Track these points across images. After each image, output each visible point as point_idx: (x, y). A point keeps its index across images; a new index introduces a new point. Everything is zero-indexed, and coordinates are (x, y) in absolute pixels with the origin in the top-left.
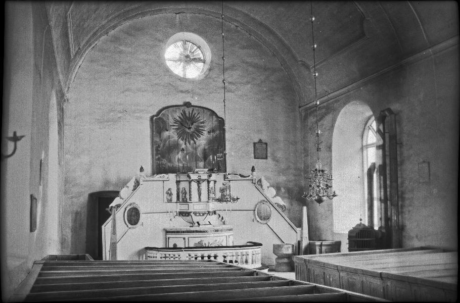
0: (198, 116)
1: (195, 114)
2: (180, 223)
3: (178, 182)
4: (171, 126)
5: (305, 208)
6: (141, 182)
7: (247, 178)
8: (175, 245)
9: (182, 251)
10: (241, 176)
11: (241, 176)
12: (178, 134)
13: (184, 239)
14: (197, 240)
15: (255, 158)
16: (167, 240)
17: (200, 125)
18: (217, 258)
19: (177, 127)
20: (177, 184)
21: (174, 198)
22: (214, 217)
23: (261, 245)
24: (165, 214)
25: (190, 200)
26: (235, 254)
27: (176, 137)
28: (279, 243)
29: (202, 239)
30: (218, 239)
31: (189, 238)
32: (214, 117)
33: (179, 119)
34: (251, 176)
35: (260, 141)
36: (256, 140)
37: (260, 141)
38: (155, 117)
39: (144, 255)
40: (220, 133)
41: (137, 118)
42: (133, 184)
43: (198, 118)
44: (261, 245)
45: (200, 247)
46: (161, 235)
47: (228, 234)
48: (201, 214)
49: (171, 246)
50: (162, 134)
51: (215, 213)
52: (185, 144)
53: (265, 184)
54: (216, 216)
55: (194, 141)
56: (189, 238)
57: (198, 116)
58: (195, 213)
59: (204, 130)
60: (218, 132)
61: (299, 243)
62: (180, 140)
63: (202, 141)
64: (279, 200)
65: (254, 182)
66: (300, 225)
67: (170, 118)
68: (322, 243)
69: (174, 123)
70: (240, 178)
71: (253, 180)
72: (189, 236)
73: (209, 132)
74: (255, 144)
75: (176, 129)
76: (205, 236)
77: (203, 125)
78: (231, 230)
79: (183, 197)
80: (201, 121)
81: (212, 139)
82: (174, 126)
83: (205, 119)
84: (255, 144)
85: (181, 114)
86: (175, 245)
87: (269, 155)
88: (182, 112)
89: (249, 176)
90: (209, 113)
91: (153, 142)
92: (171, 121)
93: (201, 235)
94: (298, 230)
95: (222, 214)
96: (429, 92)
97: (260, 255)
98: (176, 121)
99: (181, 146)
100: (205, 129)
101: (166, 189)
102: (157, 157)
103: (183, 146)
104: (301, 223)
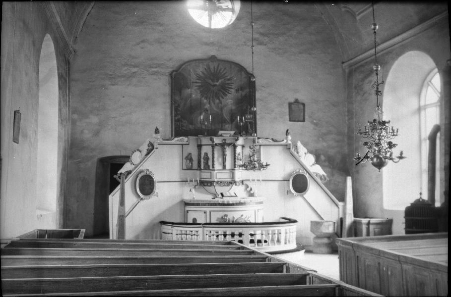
0: (225, 72)
5: (349, 180)
8: (195, 220)
13: (205, 212)
15: (290, 120)
17: (227, 82)
19: (200, 84)
27: (199, 96)
29: (226, 213)
32: (243, 73)
34: (285, 141)
35: (297, 101)
36: (292, 100)
38: (174, 73)
40: (250, 92)
42: (147, 147)
43: (225, 74)
44: (295, 221)
49: (190, 221)
52: (209, 103)
55: (220, 100)
59: (232, 88)
60: (247, 90)
62: (203, 98)
66: (342, 199)
69: (198, 79)
70: (273, 143)
73: (237, 91)
75: (198, 86)
77: (229, 82)
78: (261, 203)
80: (229, 77)
82: (196, 82)
83: (232, 76)
84: (290, 104)
86: (195, 220)
94: (341, 204)
95: (250, 185)
98: (199, 78)
100: (233, 87)
102: (176, 118)
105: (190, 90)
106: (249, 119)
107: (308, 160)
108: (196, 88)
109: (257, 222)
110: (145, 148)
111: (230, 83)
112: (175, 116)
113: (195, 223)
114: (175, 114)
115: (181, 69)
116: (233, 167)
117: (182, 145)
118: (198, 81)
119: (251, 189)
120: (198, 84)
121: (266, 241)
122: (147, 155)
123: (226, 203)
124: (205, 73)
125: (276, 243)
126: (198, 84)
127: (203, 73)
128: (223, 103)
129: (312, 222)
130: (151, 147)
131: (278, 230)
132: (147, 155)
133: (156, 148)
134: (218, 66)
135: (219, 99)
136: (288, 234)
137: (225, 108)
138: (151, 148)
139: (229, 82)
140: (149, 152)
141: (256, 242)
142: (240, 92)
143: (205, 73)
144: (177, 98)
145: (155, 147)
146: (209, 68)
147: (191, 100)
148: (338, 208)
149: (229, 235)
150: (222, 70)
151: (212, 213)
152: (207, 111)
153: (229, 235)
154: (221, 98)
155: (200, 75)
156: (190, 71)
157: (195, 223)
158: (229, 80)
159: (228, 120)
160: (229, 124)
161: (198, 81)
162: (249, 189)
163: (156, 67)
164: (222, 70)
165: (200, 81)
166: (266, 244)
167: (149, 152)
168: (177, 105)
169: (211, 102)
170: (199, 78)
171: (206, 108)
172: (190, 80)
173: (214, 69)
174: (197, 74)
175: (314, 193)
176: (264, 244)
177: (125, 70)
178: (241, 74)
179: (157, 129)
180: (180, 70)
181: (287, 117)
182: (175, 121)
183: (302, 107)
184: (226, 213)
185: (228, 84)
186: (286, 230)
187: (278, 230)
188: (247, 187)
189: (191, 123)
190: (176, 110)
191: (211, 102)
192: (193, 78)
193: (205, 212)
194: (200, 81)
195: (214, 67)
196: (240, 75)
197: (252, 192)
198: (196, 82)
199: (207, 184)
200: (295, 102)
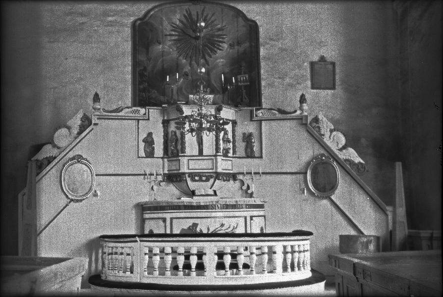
0: (213, 18)
1: (207, 16)
2: (169, 193)
3: (166, 123)
4: (166, 35)
5: (399, 166)
6: (94, 120)
7: (289, 116)
8: (151, 231)
9: (136, 241)
10: (281, 111)
11: (281, 111)
12: (178, 48)
13: (164, 220)
14: (186, 224)
15: (313, 88)
16: (142, 222)
17: (216, 33)
18: (204, 257)
19: (176, 37)
20: (164, 126)
21: (159, 150)
22: (233, 185)
23: (310, 234)
24: (142, 177)
25: (183, 153)
26: (266, 250)
27: (175, 55)
28: (353, 233)
29: (196, 221)
30: (226, 221)
31: (172, 219)
32: (240, 19)
33: (181, 25)
34: (298, 112)
35: (322, 59)
36: (316, 58)
37: (322, 59)
38: (139, 22)
39: (100, 251)
40: (251, 46)
41: (111, 24)
42: (79, 122)
43: (212, 22)
44: (310, 234)
45: (192, 233)
46: (133, 216)
47: (248, 213)
48: (204, 178)
49: (147, 232)
50: (150, 49)
51: (234, 177)
52: (190, 64)
53: (326, 126)
54: (238, 184)
55: (206, 60)
56: (172, 219)
57: (213, 18)
58: (192, 176)
59: (224, 42)
60: (247, 45)
61: (391, 234)
62: (181, 58)
63: (221, 57)
64: (352, 155)
65: (304, 122)
66: (391, 202)
67: (166, 23)
68: (432, 234)
69: (172, 30)
70: (279, 115)
71: (302, 119)
72: (174, 215)
73: (231, 46)
74: (312, 64)
75: (174, 40)
76: (208, 214)
77: (220, 33)
78: (261, 206)
79: (173, 148)
80: (219, 26)
81: (236, 55)
82: (170, 35)
83: (224, 24)
84: (312, 64)
85: (185, 16)
86: (151, 231)
87: (338, 82)
88: (185, 13)
89: (295, 111)
90: (232, 13)
91: (135, 64)
92: (167, 27)
93: (195, 215)
94: (389, 209)
95: (247, 180)
96: (410, 267)
97: (308, 254)
98: (175, 28)
99: (182, 69)
100: (225, 40)
101: (143, 135)
102: (142, 87)
103: (187, 69)
104: (134, 50)
105: (161, 46)
106: (244, 81)
107: (336, 141)
108: (170, 43)
109: (249, 232)
110: (76, 122)
111: (221, 35)
112: (139, 85)
113: (152, 234)
114: (139, 81)
115: (149, 15)
116: (215, 152)
117: (138, 120)
118: (173, 33)
119: (248, 187)
120: (173, 38)
121: (246, 266)
122: (79, 133)
123: (195, 204)
124: (184, 20)
125: (241, 269)
126: (173, 38)
127: (181, 21)
128: (210, 64)
129: (341, 236)
130: (87, 122)
131: (270, 248)
132: (79, 133)
133: (96, 124)
134: (203, 10)
135: (204, 57)
136: (289, 256)
137: (214, 71)
138: (87, 122)
139: (220, 33)
140: (82, 128)
141: (241, 266)
142: (236, 47)
143: (184, 20)
144: (142, 57)
145: (93, 122)
146: (190, 15)
147: (163, 61)
148: (387, 215)
149: (193, 255)
150: (210, 16)
151: (174, 221)
152: (187, 75)
153: (193, 255)
154: (207, 57)
155: (176, 25)
156: (162, 18)
157: (152, 234)
158: (219, 30)
159: (218, 89)
160: (220, 94)
161: (173, 33)
162: (244, 188)
163: (113, 16)
164: (210, 16)
165: (177, 33)
166: (246, 270)
167: (82, 128)
168: (142, 68)
169: (193, 62)
170: (175, 28)
171: (185, 72)
172: (162, 32)
173: (198, 15)
174: (173, 23)
175: (345, 190)
176: (242, 271)
177: (69, 21)
178: (237, 22)
179: (96, 95)
180: (147, 18)
181: (309, 83)
182: (140, 91)
183: (330, 67)
184: (196, 221)
185: (219, 36)
186: (285, 247)
187: (270, 248)
188: (242, 183)
189: (164, 94)
190: (141, 75)
191: (193, 62)
192: (166, 29)
193: (164, 220)
194: (177, 33)
195: (197, 12)
196: (236, 23)
197: (249, 192)
198: (170, 35)
199: (177, 179)
200: (320, 61)
